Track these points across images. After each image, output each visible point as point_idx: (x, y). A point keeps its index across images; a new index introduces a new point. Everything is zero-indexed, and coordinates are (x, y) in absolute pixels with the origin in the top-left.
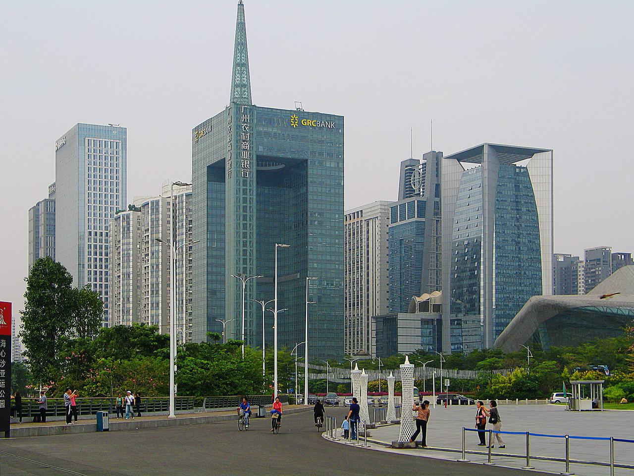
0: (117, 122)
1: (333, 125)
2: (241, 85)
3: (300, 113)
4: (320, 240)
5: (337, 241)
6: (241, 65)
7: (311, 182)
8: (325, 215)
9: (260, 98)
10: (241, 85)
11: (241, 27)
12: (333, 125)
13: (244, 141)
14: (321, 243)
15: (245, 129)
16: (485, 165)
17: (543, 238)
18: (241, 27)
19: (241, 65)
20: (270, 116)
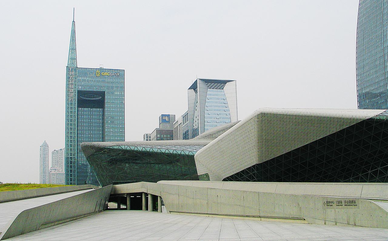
0: (110, 64)
1: (118, 75)
2: (73, 58)
3: (101, 69)
4: (111, 130)
5: (121, 130)
6: (73, 49)
7: (108, 102)
8: (114, 118)
9: (81, 64)
10: (73, 58)
11: (73, 32)
12: (118, 75)
13: (71, 84)
14: (112, 132)
16: (154, 142)
17: (239, 183)
18: (73, 32)
19: (73, 49)
20: (86, 72)
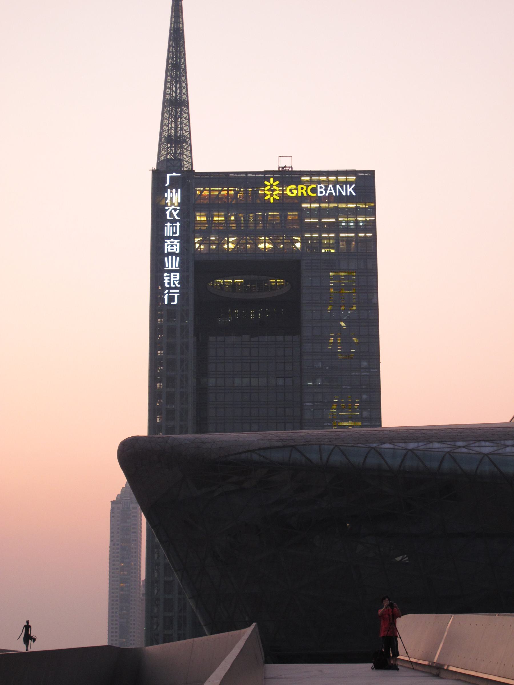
2: (175, 140)
9: (207, 156)
10: (175, 140)
15: (171, 215)
